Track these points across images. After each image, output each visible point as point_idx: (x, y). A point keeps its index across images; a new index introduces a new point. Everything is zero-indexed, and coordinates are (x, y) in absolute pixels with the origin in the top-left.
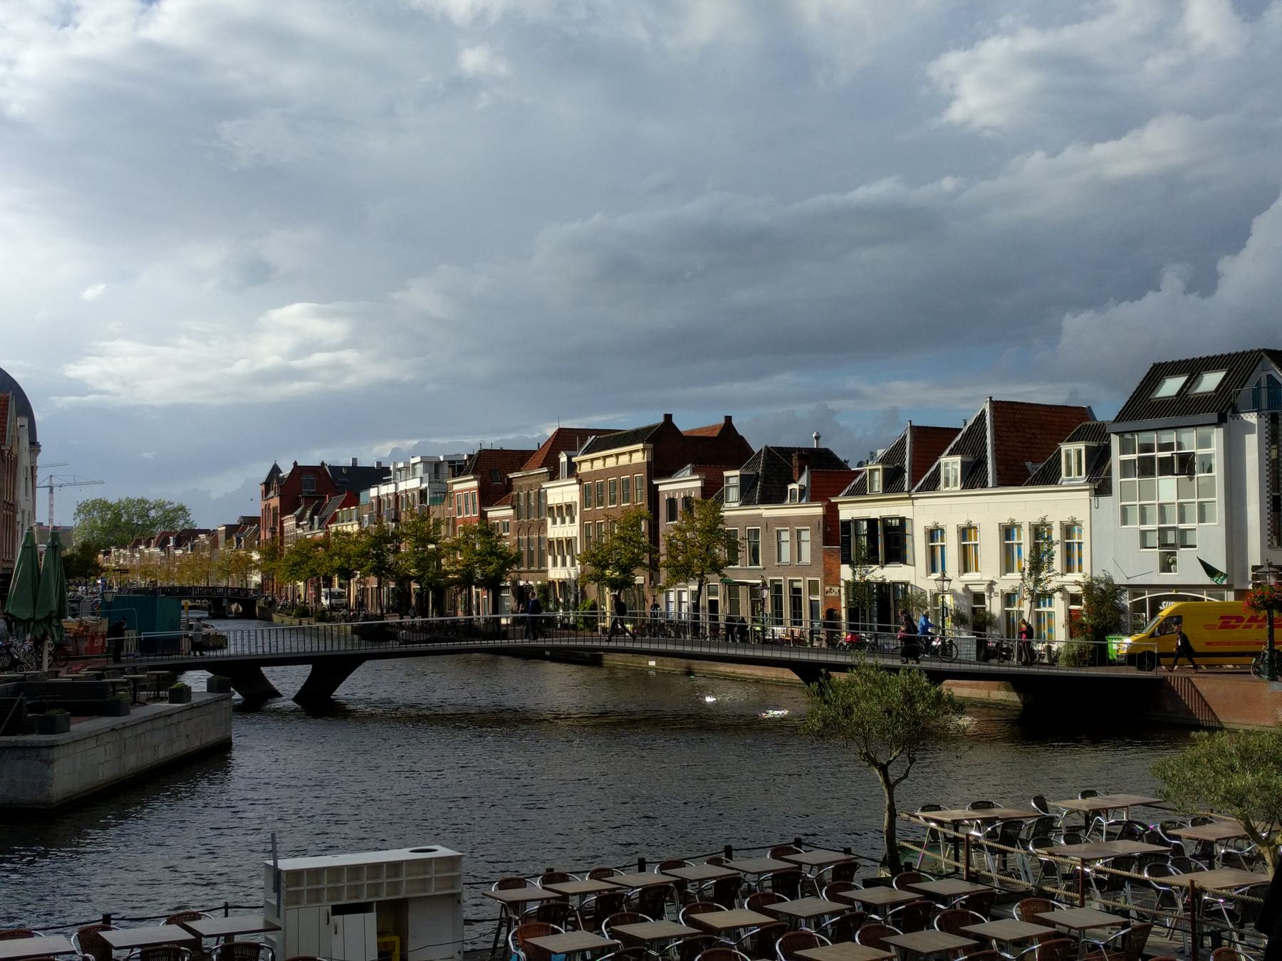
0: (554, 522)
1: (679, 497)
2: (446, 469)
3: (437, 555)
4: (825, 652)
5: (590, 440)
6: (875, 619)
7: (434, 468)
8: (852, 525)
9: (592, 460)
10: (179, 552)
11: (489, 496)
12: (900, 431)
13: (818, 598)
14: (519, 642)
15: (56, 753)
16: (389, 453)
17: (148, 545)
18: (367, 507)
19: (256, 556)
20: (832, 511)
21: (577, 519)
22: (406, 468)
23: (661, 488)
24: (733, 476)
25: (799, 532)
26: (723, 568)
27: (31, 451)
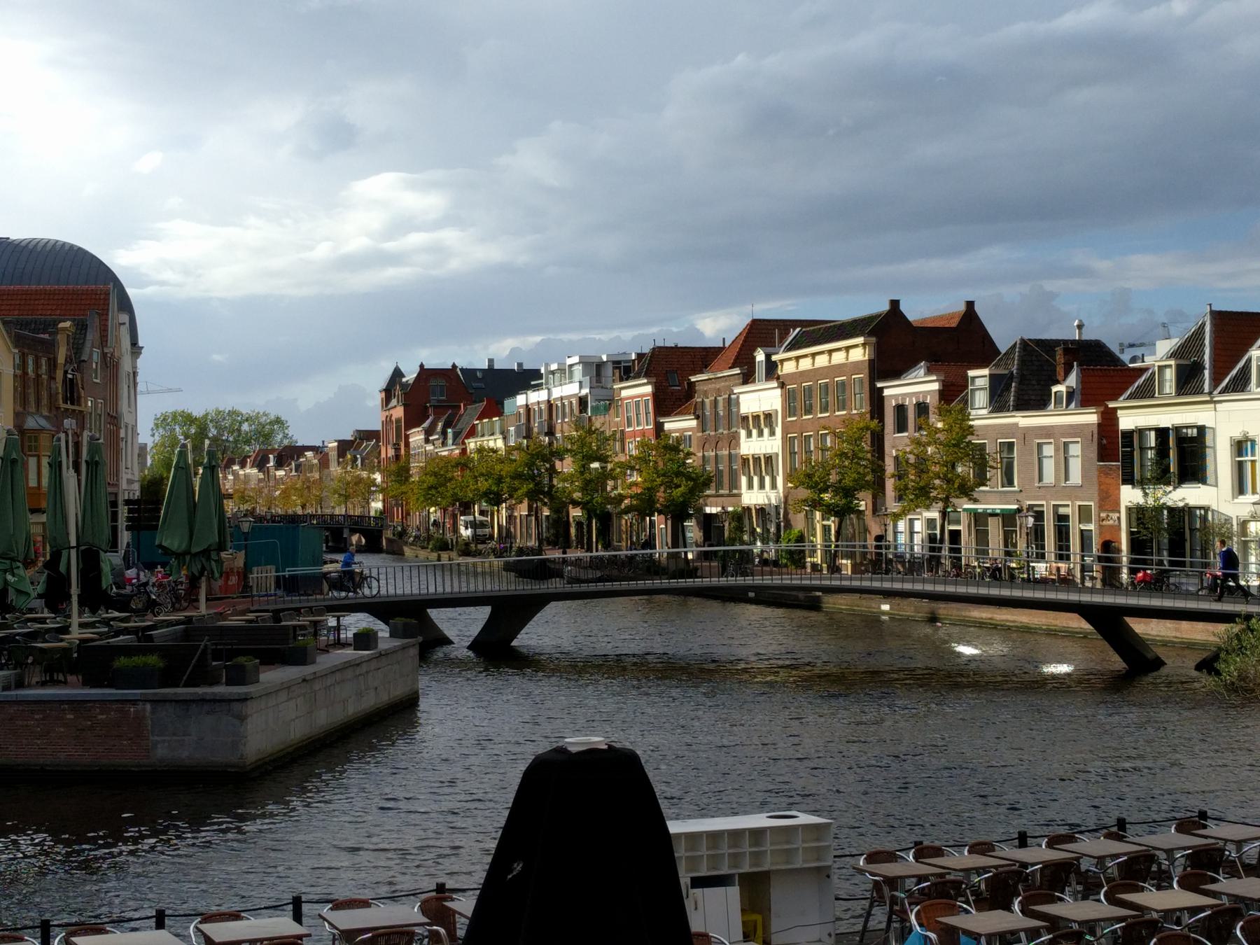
0: (749, 435)
1: (910, 403)
2: (609, 370)
3: (604, 476)
4: (1102, 592)
5: (793, 333)
6: (1165, 553)
7: (595, 370)
8: (1136, 437)
9: (798, 358)
10: (281, 473)
11: (666, 403)
12: (1197, 315)
13: (1091, 527)
14: (706, 581)
15: (250, 708)
16: (507, 352)
17: (243, 466)
18: (513, 418)
19: (378, 477)
20: (1109, 419)
21: (779, 430)
22: (561, 370)
23: (886, 392)
24: (980, 376)
25: (1066, 445)
26: (973, 490)
27: (133, 353)
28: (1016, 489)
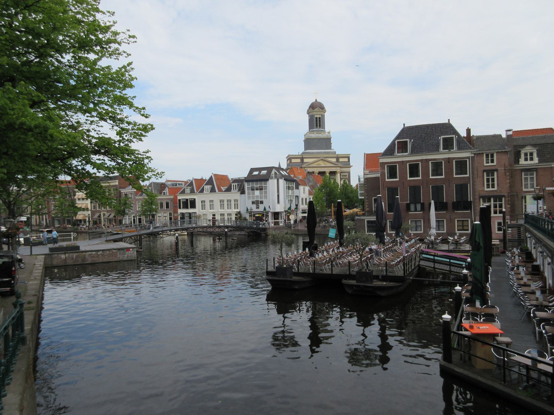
23: (121, 191)
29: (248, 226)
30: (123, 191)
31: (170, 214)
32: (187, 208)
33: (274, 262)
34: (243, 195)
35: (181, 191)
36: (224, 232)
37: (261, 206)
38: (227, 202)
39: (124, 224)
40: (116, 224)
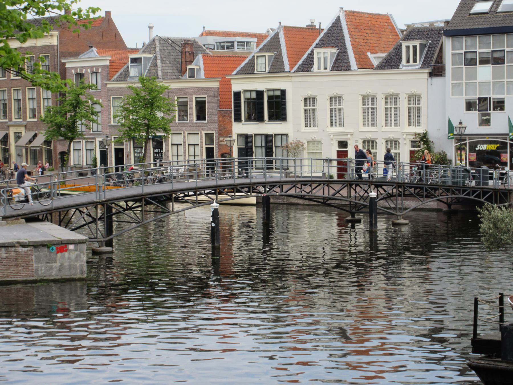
23: (67, 66)
28: (206, 122)
29: (450, 182)
30: (71, 64)
31: (209, 137)
32: (260, 118)
33: (501, 310)
34: (436, 80)
35: (243, 64)
36: (368, 200)
37: (495, 115)
38: (386, 103)
39: (75, 167)
40: (51, 164)
